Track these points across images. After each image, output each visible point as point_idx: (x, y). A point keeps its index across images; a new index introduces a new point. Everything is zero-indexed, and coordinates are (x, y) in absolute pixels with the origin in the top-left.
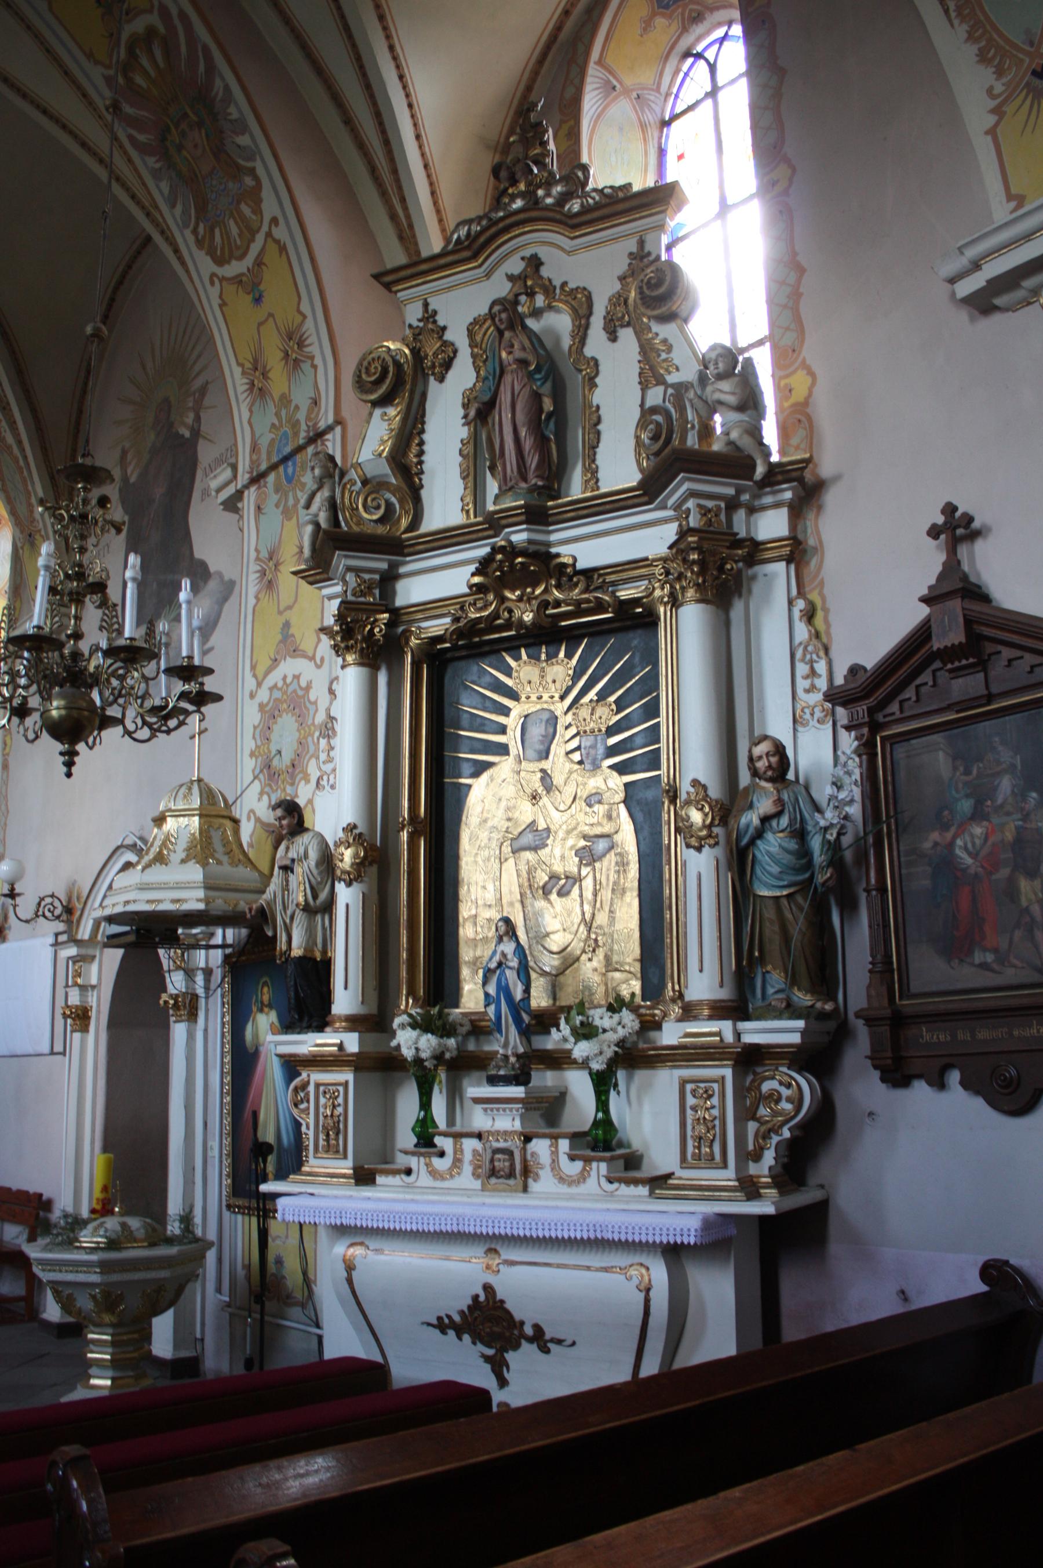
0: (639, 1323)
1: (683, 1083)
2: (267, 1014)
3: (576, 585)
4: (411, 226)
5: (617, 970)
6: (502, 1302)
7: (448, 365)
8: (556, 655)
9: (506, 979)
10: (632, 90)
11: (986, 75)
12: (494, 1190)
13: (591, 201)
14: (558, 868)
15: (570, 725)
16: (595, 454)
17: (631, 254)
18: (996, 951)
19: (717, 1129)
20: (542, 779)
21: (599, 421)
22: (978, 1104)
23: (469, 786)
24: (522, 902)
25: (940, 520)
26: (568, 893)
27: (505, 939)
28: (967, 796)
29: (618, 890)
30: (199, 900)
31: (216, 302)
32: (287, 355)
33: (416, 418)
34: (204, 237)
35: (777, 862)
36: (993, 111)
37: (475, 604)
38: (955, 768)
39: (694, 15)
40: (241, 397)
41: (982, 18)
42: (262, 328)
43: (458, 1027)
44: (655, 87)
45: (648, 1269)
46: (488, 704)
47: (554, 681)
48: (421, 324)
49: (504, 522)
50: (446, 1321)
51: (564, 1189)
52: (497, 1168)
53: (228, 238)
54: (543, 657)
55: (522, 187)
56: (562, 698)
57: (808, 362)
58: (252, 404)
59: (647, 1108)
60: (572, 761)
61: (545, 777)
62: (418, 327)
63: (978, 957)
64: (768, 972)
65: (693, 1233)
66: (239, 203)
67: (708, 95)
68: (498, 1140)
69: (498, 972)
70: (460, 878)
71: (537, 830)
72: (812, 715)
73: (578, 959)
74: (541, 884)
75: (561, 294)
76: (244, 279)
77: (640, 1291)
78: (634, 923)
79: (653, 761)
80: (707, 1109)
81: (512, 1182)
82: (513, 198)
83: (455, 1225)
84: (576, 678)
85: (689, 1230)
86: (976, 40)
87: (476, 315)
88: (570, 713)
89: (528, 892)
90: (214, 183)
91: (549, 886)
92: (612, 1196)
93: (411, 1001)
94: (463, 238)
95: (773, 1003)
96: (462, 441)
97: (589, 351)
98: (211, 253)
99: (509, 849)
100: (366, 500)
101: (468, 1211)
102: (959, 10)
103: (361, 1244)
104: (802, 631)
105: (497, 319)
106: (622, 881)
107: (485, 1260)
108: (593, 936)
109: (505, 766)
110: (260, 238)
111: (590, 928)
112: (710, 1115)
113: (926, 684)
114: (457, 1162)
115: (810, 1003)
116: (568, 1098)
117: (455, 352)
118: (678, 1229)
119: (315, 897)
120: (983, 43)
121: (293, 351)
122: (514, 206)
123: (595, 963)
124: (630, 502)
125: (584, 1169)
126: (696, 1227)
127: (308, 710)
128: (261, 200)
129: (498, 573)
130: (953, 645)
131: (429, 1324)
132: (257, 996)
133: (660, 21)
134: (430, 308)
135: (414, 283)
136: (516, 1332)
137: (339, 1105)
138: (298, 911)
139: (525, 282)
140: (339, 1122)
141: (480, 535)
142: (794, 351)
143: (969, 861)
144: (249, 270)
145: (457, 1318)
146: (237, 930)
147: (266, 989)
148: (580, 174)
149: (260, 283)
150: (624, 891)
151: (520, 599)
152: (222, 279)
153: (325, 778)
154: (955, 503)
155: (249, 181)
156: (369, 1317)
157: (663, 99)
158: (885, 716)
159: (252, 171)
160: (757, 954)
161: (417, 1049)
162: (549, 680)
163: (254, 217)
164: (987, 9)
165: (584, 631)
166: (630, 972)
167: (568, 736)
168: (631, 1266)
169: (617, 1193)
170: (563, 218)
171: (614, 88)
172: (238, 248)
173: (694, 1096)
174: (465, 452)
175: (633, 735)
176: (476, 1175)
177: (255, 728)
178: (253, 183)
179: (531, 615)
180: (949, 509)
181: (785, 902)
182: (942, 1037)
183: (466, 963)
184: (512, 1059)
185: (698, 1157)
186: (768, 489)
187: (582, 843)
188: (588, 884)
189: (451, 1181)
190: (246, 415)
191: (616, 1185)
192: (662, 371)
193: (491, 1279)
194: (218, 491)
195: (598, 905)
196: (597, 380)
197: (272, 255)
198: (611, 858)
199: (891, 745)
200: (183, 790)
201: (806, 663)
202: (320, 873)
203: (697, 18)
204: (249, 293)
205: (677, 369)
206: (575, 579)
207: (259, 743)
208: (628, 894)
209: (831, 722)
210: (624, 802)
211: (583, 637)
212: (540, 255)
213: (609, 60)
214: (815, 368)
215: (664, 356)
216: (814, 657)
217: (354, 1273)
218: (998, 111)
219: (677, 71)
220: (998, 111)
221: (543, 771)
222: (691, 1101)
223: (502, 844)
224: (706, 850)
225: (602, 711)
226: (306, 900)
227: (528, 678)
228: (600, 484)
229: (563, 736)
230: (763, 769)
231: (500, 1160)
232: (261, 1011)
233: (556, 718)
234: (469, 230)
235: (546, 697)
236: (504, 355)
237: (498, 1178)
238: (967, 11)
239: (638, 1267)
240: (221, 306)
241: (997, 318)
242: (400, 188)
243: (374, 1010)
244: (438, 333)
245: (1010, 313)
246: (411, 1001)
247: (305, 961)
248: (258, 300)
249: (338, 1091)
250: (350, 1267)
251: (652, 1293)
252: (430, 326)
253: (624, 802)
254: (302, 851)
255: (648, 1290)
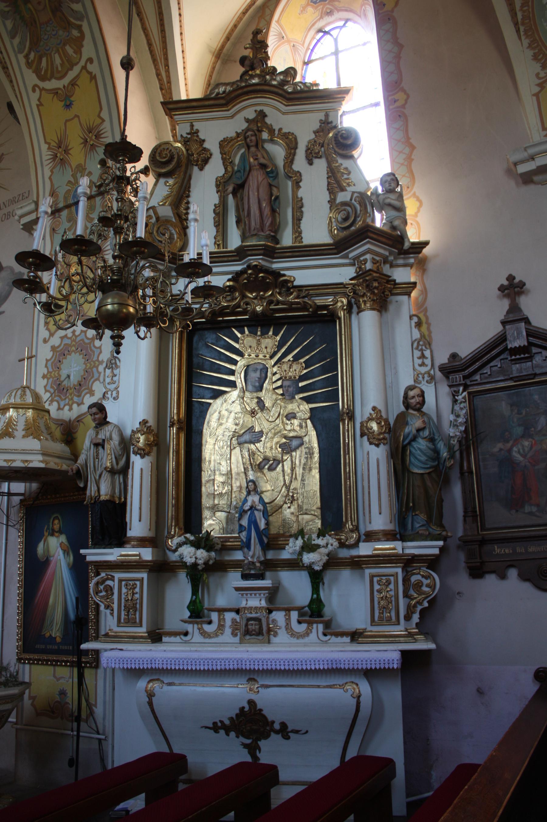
0: (352, 716)
1: (372, 577)
2: (57, 537)
3: (292, 293)
4: (169, 82)
5: (306, 514)
6: (261, 710)
7: (206, 161)
8: (268, 333)
9: (255, 517)
10: (291, 41)
11: (537, 67)
12: (249, 643)
13: (299, 88)
14: (269, 454)
15: (276, 373)
16: (300, 223)
17: (321, 120)
18: (538, 505)
19: (393, 603)
20: (258, 403)
21: (302, 206)
22: (527, 587)
23: (210, 404)
24: (245, 473)
25: (506, 283)
26: (275, 469)
27: (252, 493)
28: (519, 425)
29: (307, 468)
30: (41, 462)
31: (34, 103)
32: (86, 141)
33: (185, 188)
34: (33, 61)
35: (425, 454)
36: (538, 85)
37: (226, 298)
38: (512, 411)
39: (328, 11)
40: (45, 163)
41: (538, 38)
42: (68, 123)
43: (216, 545)
44: (302, 43)
45: (357, 685)
46: (222, 357)
47: (266, 348)
48: (189, 136)
49: (249, 253)
50: (219, 724)
51: (294, 640)
52: (251, 630)
53: (52, 64)
54: (259, 333)
55: (258, 72)
56: (271, 357)
57: (417, 194)
58: (54, 168)
59: (334, 592)
60: (277, 394)
61: (260, 403)
62: (187, 137)
63: (527, 509)
64: (416, 515)
65: (396, 662)
66: (65, 45)
67: (332, 54)
68: (251, 613)
69: (249, 513)
70: (203, 458)
71: (255, 432)
72: (423, 378)
73: (281, 507)
74: (258, 463)
75: (278, 134)
76: (60, 92)
77: (354, 698)
78: (317, 488)
79: (333, 396)
80: (387, 591)
81: (260, 637)
82: (252, 77)
83: (236, 665)
84: (280, 347)
85: (393, 660)
86: (533, 49)
87: (225, 137)
88: (276, 367)
89: (250, 467)
90: (48, 29)
91: (263, 464)
92: (327, 643)
93: (177, 530)
94: (221, 92)
95: (420, 532)
96: (215, 205)
97: (296, 167)
98: (37, 72)
99: (236, 442)
100: (159, 228)
101: (245, 656)
102: (526, 31)
103: (158, 680)
104: (416, 334)
105: (248, 140)
106: (309, 463)
107: (248, 686)
108: (291, 494)
109: (234, 394)
110: (77, 69)
111: (289, 489)
112: (390, 595)
113: (497, 366)
114: (221, 627)
115: (439, 532)
116: (280, 588)
117: (211, 155)
118: (386, 660)
119: (117, 464)
120: (537, 51)
121: (91, 139)
122: (254, 81)
123: (292, 509)
124: (325, 252)
125: (308, 628)
126: (398, 658)
127: (94, 352)
128: (82, 46)
129: (245, 281)
130: (520, 346)
131: (207, 727)
132: (49, 526)
133: (310, 9)
134: (195, 128)
135: (186, 112)
136: (268, 728)
137: (137, 593)
138: (104, 472)
139: (257, 124)
140: (136, 604)
141: (230, 259)
142: (408, 187)
143: (521, 459)
144: (64, 87)
145: (227, 722)
146: (28, 484)
147: (56, 522)
148: (292, 72)
149: (72, 96)
150: (310, 469)
151: (255, 298)
152: (42, 90)
153: (109, 393)
154: (514, 274)
155: (75, 33)
156: (163, 726)
157: (305, 50)
158: (471, 381)
159: (79, 28)
160: (411, 505)
161: (196, 558)
162: (263, 346)
163: (75, 55)
164: (541, 35)
165: (286, 321)
166: (315, 515)
167: (274, 379)
168: (346, 683)
169: (329, 641)
170: (284, 93)
171: (283, 37)
172: (58, 72)
173: (379, 584)
174: (218, 211)
175: (315, 381)
176: (234, 634)
177: (47, 361)
178: (79, 35)
179: (261, 308)
180: (511, 278)
181: (426, 476)
182: (507, 551)
183: (207, 508)
184: (258, 565)
185: (381, 619)
186: (402, 256)
187: (284, 440)
188: (287, 466)
189: (216, 638)
190: (47, 173)
191: (328, 637)
192: (344, 184)
193: (253, 697)
194: (21, 216)
195: (294, 476)
196: (301, 184)
197: (85, 78)
198: (303, 449)
199: (473, 396)
200: (19, 392)
201: (419, 351)
202: (121, 449)
203: (330, 13)
204: (62, 101)
205: (354, 185)
206: (292, 290)
207: (50, 370)
208: (313, 471)
209: (434, 383)
210: (310, 418)
211: (284, 325)
212: (265, 111)
213: (283, 22)
214: (421, 198)
215: (345, 176)
216: (424, 348)
217: (154, 699)
218: (540, 85)
219: (313, 38)
220: (540, 85)
221: (259, 398)
222: (377, 587)
223: (232, 439)
224: (382, 446)
225: (295, 366)
226: (112, 465)
227: (249, 344)
228: (303, 240)
229: (271, 379)
230: (415, 404)
231: (252, 624)
232: (52, 535)
233: (267, 368)
234: (226, 89)
235: (261, 356)
236: (252, 160)
237: (251, 635)
238: (530, 33)
239: (351, 684)
240: (38, 106)
241: (532, 187)
242: (166, 59)
243: (154, 536)
244: (200, 143)
245: (540, 186)
246: (177, 530)
247: (110, 502)
248: (68, 106)
249: (136, 584)
250: (150, 695)
251: (361, 699)
252: (195, 138)
253: (310, 418)
254: (108, 434)
255: (359, 697)
